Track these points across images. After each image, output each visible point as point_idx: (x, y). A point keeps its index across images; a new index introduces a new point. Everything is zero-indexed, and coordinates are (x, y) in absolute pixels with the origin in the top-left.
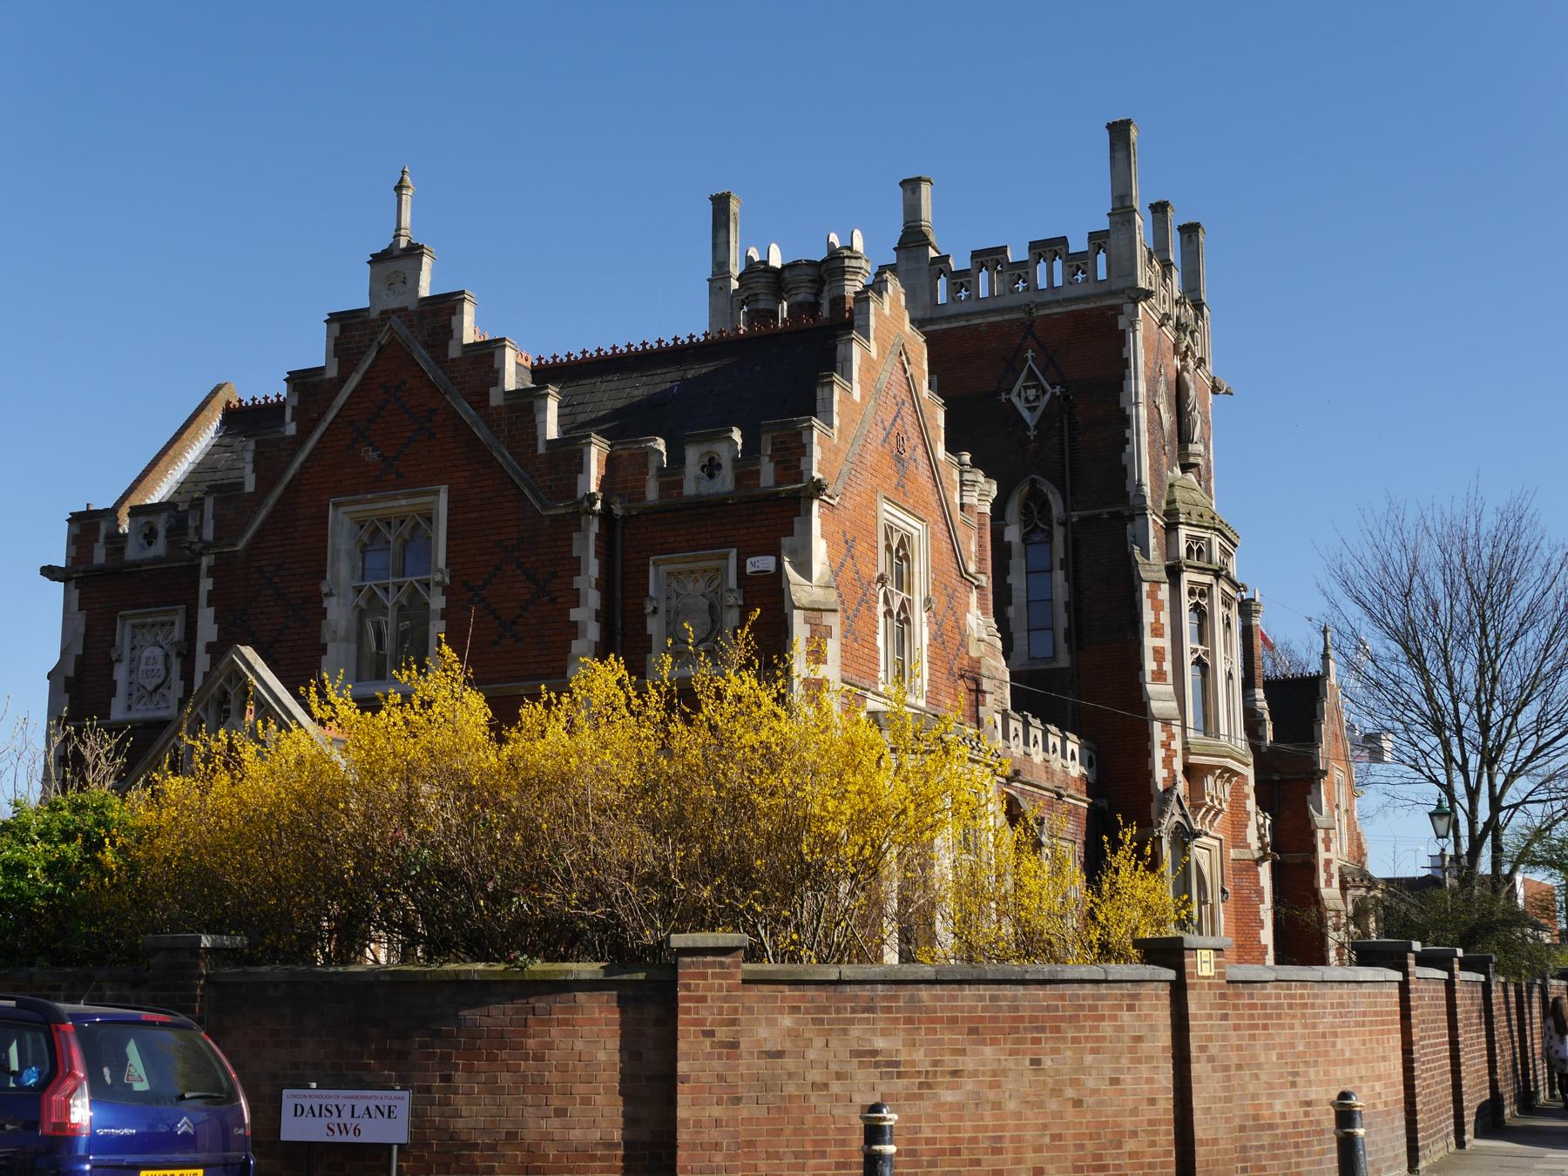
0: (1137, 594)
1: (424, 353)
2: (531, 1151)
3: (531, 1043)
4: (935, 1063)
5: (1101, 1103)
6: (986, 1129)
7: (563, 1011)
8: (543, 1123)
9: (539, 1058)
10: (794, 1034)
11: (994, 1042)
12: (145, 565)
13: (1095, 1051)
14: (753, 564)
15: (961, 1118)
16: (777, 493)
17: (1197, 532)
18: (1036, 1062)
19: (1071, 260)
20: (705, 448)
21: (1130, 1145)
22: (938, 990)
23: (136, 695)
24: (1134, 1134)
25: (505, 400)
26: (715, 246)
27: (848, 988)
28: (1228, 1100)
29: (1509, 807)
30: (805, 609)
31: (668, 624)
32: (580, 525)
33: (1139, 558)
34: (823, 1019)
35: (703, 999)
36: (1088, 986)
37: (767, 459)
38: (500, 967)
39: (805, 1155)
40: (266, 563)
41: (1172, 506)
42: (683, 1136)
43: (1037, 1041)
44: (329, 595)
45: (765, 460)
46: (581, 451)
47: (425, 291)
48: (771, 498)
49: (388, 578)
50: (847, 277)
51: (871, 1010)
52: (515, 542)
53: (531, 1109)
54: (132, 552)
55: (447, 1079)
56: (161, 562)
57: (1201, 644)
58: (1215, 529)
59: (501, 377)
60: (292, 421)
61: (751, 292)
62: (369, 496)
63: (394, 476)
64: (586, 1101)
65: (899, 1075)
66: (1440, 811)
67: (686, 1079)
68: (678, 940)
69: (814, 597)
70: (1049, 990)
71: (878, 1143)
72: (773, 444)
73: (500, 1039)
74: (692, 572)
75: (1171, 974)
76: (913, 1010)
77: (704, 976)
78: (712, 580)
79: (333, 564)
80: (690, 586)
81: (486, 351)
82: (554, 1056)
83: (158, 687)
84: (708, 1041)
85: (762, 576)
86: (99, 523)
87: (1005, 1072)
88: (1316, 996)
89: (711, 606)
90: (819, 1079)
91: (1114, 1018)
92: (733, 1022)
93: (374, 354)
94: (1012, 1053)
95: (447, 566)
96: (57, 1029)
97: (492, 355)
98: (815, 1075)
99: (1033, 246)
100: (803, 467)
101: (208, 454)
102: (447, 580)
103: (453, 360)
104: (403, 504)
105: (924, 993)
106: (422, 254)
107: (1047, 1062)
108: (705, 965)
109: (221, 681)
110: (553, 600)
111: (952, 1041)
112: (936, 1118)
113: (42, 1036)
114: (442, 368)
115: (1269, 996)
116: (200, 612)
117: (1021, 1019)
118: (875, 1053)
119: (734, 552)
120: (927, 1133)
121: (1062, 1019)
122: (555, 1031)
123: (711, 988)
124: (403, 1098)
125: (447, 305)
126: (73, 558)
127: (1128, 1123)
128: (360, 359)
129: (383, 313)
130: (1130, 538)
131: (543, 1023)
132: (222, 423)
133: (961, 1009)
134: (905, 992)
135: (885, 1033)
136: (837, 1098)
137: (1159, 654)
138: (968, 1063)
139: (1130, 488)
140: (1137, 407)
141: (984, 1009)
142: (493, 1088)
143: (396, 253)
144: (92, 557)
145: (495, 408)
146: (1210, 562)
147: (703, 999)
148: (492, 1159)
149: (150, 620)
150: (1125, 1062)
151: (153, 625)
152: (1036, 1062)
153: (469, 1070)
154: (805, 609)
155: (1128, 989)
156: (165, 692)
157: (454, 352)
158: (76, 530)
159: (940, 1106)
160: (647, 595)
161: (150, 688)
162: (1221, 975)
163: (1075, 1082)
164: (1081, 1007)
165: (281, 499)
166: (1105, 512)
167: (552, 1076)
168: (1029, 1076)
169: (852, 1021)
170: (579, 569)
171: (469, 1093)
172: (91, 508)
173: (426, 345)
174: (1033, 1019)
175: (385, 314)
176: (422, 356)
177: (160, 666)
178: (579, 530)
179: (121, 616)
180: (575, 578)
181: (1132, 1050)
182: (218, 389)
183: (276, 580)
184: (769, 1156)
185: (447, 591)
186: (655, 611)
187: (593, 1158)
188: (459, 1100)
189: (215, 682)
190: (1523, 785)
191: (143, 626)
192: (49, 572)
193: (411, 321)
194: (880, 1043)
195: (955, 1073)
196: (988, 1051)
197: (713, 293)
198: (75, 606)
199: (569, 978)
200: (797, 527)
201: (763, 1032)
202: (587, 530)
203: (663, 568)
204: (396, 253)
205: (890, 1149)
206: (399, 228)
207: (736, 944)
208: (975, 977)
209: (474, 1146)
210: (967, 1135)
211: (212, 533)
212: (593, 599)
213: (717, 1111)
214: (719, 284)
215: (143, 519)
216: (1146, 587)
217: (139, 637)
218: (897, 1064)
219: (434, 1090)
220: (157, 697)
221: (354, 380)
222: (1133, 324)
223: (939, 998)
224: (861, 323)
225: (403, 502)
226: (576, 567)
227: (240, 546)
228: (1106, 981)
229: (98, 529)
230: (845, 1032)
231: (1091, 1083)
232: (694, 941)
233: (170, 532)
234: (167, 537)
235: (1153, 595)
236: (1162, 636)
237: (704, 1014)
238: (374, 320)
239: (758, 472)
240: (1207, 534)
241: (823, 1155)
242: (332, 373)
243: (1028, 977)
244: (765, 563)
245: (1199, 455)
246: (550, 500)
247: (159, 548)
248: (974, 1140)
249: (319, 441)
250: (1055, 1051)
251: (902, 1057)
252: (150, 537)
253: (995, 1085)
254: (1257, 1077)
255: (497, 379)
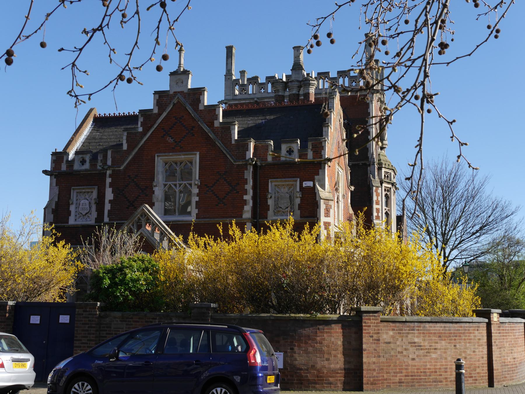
0: (371, 191)
1: (190, 107)
2: (319, 371)
3: (318, 339)
4: (430, 346)
5: (471, 358)
6: (443, 365)
7: (328, 329)
8: (322, 362)
9: (321, 343)
10: (393, 337)
11: (445, 340)
12: (82, 172)
13: (469, 343)
14: (305, 184)
15: (437, 362)
16: (314, 162)
17: (387, 170)
18: (455, 346)
19: (352, 78)
20: (289, 145)
21: (478, 370)
22: (431, 324)
23: (78, 216)
24: (479, 367)
25: (220, 125)
26: (227, 64)
27: (407, 323)
28: (500, 357)
29: (450, 260)
30: (324, 199)
31: (275, 201)
32: (247, 168)
33: (372, 179)
34: (401, 333)
35: (370, 326)
36: (467, 324)
37: (310, 150)
38: (309, 315)
39: (397, 373)
40: (131, 174)
41: (380, 162)
42: (365, 367)
43: (455, 340)
44: (156, 186)
45: (309, 150)
46: (248, 144)
47: (189, 87)
48: (311, 163)
49: (176, 181)
50: (310, 86)
51: (413, 330)
52: (224, 172)
53: (318, 358)
54: (77, 167)
55: (292, 349)
56: (88, 171)
57: (387, 207)
58: (392, 170)
59: (218, 117)
60: (141, 126)
61: (277, 89)
62: (171, 154)
63: (179, 148)
64: (335, 356)
65: (421, 349)
66: (466, 264)
67: (365, 350)
68: (364, 308)
69: (326, 196)
70: (458, 325)
71: (461, 370)
72: (312, 145)
73: (308, 337)
74: (283, 185)
75: (487, 320)
76: (424, 330)
77: (370, 319)
78: (290, 188)
79: (157, 176)
80: (282, 190)
81: (213, 108)
82: (325, 343)
83: (86, 214)
84: (371, 339)
85: (308, 188)
86: (63, 156)
87: (447, 349)
88: (515, 327)
89: (290, 196)
90: (400, 350)
91: (474, 333)
92: (378, 333)
93: (172, 106)
94: (449, 343)
95: (199, 179)
96: (245, 335)
97: (215, 110)
98: (399, 349)
99: (339, 72)
100: (322, 153)
101: (91, 133)
102: (199, 184)
103: (201, 110)
104: (182, 157)
105: (427, 325)
106: (189, 74)
107: (458, 346)
108: (370, 316)
109: (139, 216)
110: (238, 192)
111: (435, 340)
112: (431, 362)
113: (240, 337)
114: (197, 113)
115: (506, 327)
116: (106, 189)
117: (451, 333)
118: (415, 343)
119: (299, 179)
120: (428, 367)
121: (461, 333)
122: (325, 335)
123: (372, 323)
124: (281, 355)
125: (198, 92)
126: (53, 168)
127: (477, 364)
128: (166, 108)
129: (175, 92)
130: (369, 172)
131: (321, 332)
132: (93, 122)
133: (436, 330)
134: (422, 325)
135: (418, 337)
136: (405, 356)
137: (378, 210)
138: (438, 346)
139: (369, 155)
140: (372, 129)
141: (442, 330)
142: (306, 352)
143: (179, 72)
144: (61, 168)
145: (216, 127)
146: (391, 180)
147: (370, 326)
148: (307, 373)
149: (84, 191)
150: (476, 347)
151: (84, 192)
152: (455, 346)
153: (299, 346)
154: (324, 199)
155: (477, 325)
156: (89, 215)
157: (201, 108)
158: (54, 158)
159: (432, 359)
160: (268, 192)
161: (84, 214)
162: (498, 321)
163: (465, 352)
164: (466, 330)
165: (136, 153)
166: (361, 163)
167: (325, 349)
168: (453, 350)
169: (408, 333)
170: (247, 182)
171: (299, 354)
172: (57, 151)
173: (191, 104)
174: (454, 333)
175: (176, 93)
176: (189, 108)
177: (88, 206)
178: (247, 170)
179: (73, 189)
180: (246, 185)
181: (478, 343)
182: (91, 110)
183: (135, 180)
184: (387, 373)
185: (199, 187)
186: (271, 197)
187: (338, 373)
188: (296, 356)
189: (136, 216)
190: (455, 252)
191: (81, 192)
192: (45, 172)
193: (186, 96)
194: (416, 340)
195: (435, 349)
196: (443, 342)
197: (226, 80)
198: (54, 184)
199: (330, 319)
200: (320, 173)
201: (385, 336)
202: (250, 170)
203: (273, 184)
204: (179, 72)
205: (464, 371)
206: (180, 64)
207: (379, 310)
208: (441, 321)
209: (301, 369)
210: (438, 367)
211: (111, 162)
212: (251, 192)
213: (374, 360)
214: (228, 77)
215: (80, 156)
216: (374, 188)
217: (79, 196)
218: (420, 346)
219: (288, 352)
220: (86, 217)
221: (164, 114)
222: (372, 101)
223: (431, 327)
224: (331, 106)
225: (183, 157)
226: (246, 182)
227: (122, 168)
228: (472, 322)
229: (63, 158)
230: (407, 336)
231: (468, 352)
232: (368, 309)
233: (91, 161)
234: (90, 162)
235: (376, 191)
236: (379, 204)
237: (370, 331)
238: (171, 95)
239: (307, 154)
240: (390, 171)
241: (401, 373)
242: (156, 111)
243: (454, 321)
244: (310, 184)
245: (386, 145)
246: (236, 159)
247: (87, 166)
248: (440, 369)
249: (151, 134)
250: (460, 343)
251: (422, 344)
252: (83, 162)
253: (445, 353)
254: (504, 350)
255: (217, 118)
